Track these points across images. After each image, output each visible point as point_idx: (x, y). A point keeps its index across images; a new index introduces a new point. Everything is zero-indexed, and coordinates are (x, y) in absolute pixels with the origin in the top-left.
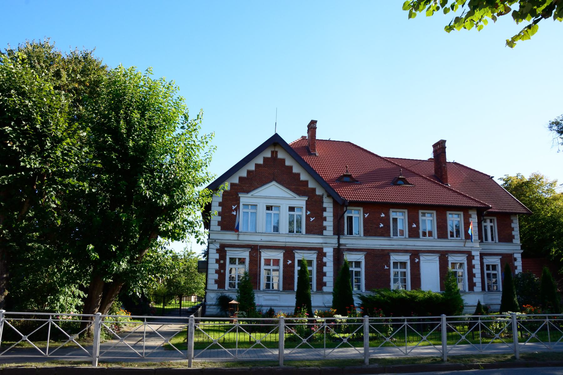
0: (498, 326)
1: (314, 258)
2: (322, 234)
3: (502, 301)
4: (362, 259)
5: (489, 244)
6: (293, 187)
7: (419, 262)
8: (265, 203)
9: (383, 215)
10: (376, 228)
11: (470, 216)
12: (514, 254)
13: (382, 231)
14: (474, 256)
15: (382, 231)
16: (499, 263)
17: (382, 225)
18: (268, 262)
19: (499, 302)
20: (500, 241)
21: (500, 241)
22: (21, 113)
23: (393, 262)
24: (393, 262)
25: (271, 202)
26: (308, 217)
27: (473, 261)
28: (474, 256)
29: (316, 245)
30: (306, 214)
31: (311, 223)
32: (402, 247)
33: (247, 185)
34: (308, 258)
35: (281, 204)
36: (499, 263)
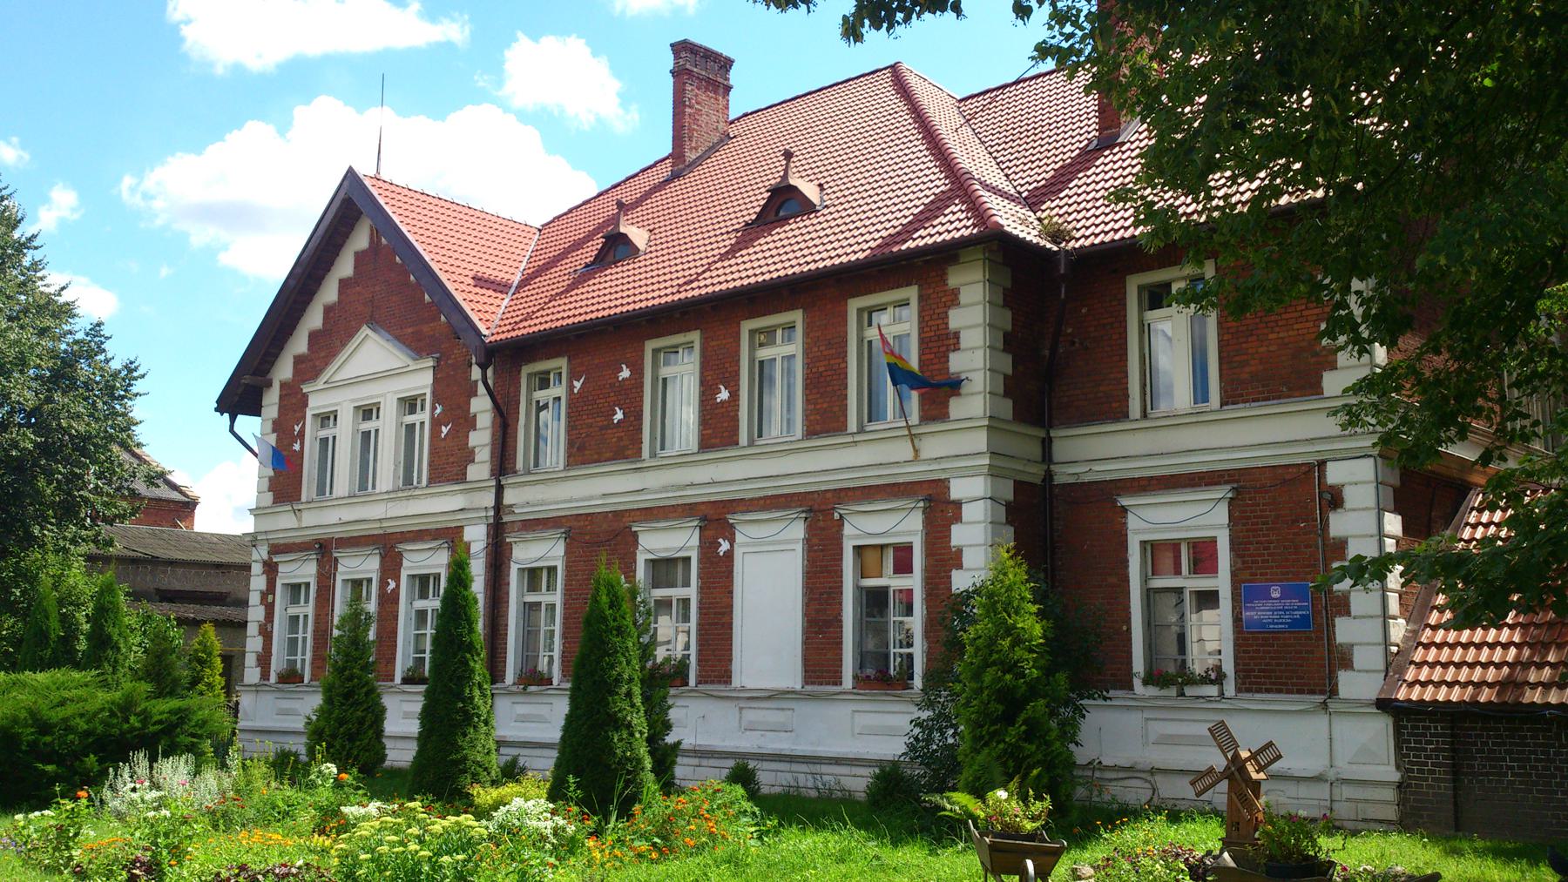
0: (364, 833)
1: (910, 533)
2: (461, 477)
3: (567, 729)
4: (689, 549)
5: (1176, 421)
6: (410, 330)
7: (730, 555)
8: (395, 393)
9: (625, 373)
10: (601, 428)
11: (953, 299)
12: (1322, 464)
13: (620, 439)
14: (958, 504)
15: (620, 439)
16: (1220, 527)
17: (619, 415)
18: (1160, 553)
19: (554, 733)
20: (1230, 397)
21: (1230, 397)
22: (1258, 132)
23: (1143, 543)
24: (1143, 543)
25: (365, 394)
26: (436, 423)
27: (956, 530)
28: (958, 504)
29: (632, 499)
30: (304, 423)
31: (443, 444)
32: (670, 495)
33: (323, 354)
34: (1188, 529)
35: (337, 404)
36: (1220, 527)
